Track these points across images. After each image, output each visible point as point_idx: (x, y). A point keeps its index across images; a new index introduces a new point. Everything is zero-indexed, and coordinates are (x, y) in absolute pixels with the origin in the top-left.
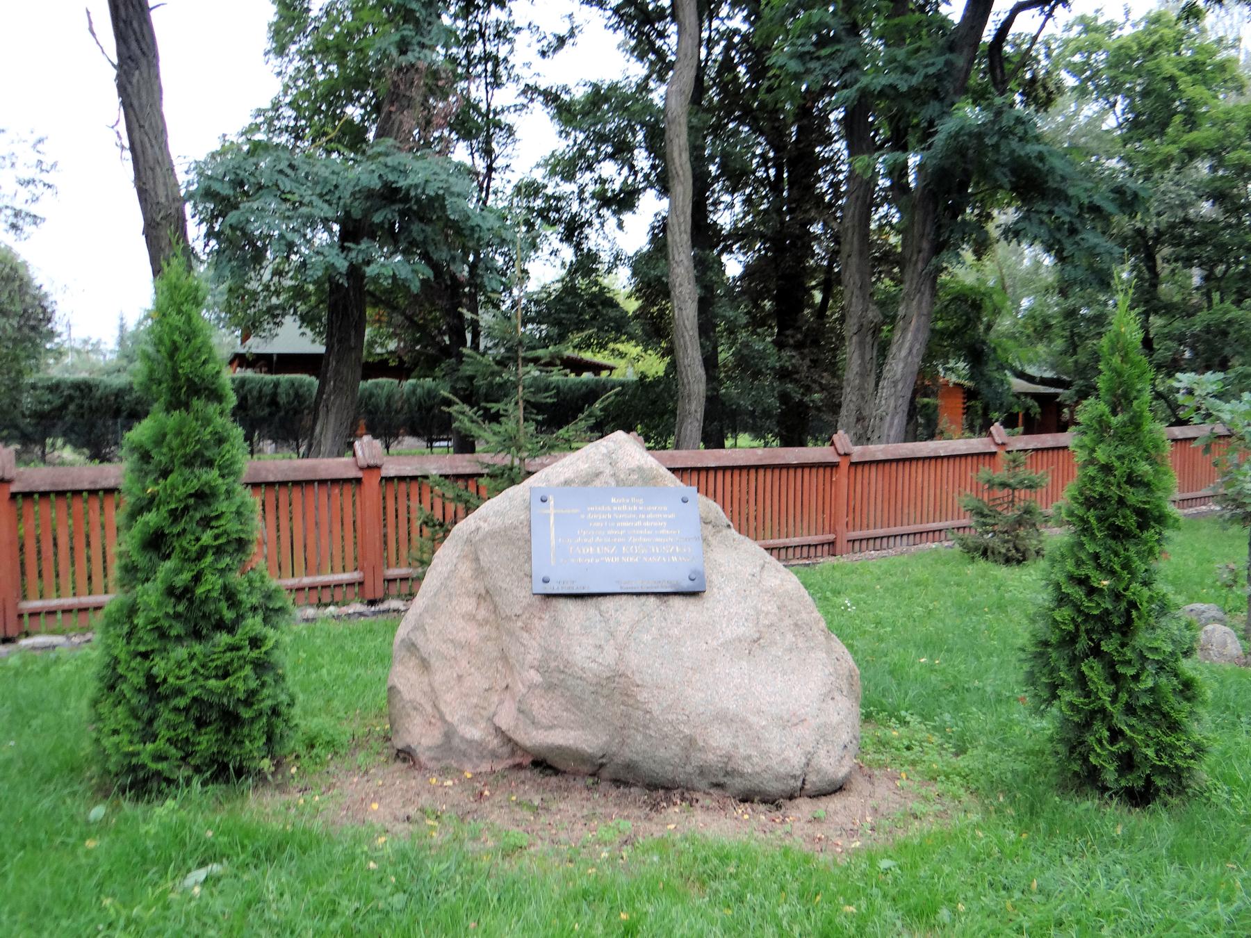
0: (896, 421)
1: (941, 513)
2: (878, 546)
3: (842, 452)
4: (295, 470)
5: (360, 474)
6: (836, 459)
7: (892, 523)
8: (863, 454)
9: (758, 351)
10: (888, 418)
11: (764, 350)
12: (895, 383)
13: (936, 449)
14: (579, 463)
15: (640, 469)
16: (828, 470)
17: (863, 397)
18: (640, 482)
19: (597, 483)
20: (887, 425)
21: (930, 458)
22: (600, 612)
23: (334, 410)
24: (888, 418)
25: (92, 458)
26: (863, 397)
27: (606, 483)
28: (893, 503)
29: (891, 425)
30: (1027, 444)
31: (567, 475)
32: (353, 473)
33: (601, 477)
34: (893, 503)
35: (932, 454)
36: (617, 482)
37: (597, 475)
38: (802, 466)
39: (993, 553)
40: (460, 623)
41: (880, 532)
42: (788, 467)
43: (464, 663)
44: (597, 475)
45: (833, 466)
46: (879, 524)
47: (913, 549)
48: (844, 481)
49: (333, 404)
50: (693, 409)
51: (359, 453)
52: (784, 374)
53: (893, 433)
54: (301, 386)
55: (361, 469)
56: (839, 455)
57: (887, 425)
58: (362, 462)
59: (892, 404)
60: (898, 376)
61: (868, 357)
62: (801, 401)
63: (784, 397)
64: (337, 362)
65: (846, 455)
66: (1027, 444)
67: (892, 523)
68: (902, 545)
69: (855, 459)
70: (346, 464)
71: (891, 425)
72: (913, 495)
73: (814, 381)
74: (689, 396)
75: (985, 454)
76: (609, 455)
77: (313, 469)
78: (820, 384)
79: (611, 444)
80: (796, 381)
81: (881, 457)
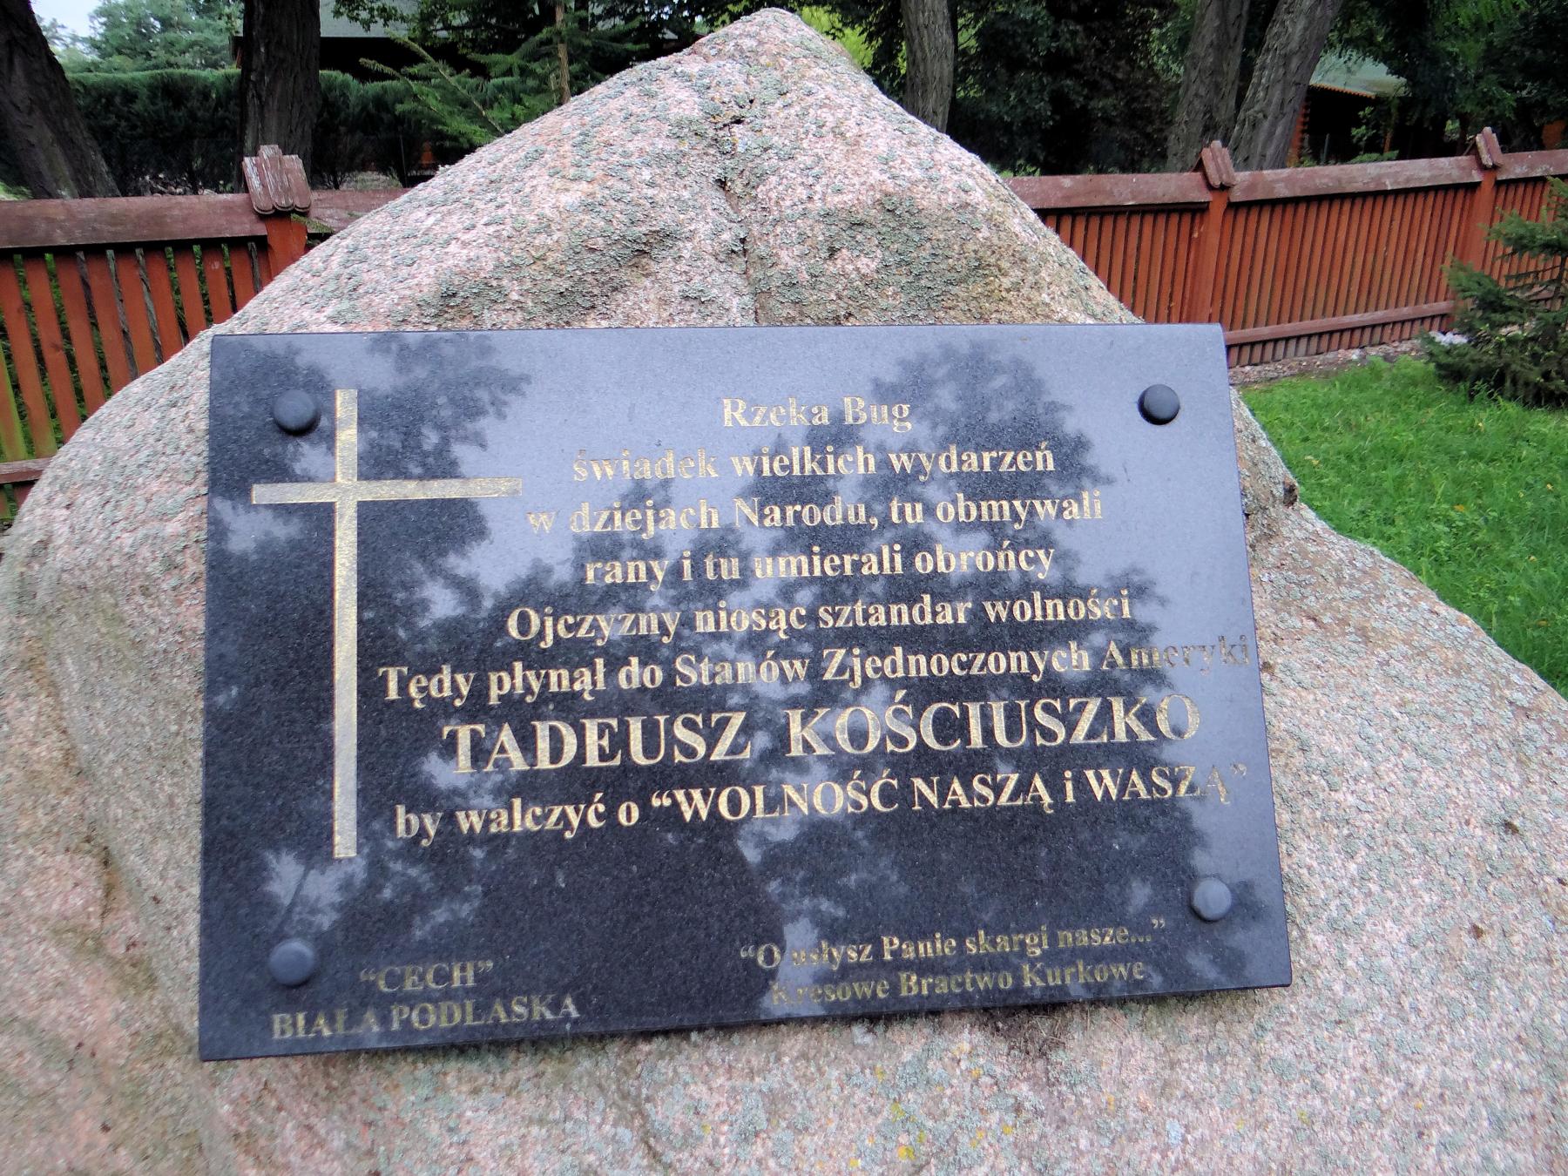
0: (1279, 130)
1: (1368, 296)
2: (1256, 358)
3: (1216, 183)
4: (115, 219)
5: (261, 230)
6: (1203, 196)
7: (1285, 316)
8: (1252, 187)
9: (1024, 21)
10: (1266, 124)
11: (1034, 21)
12: (1287, 58)
13: (1379, 178)
14: (538, 177)
15: (897, 214)
16: (1187, 219)
17: (1217, 86)
18: (890, 298)
19: (642, 300)
20: (1262, 136)
21: (1364, 195)
22: (648, 1140)
23: (274, 104)
24: (1266, 124)
25: (36, 196)
26: (1217, 86)
27: (696, 300)
28: (1291, 278)
29: (1271, 134)
30: (1532, 167)
31: (457, 256)
32: (246, 227)
33: (663, 267)
34: (1291, 278)
35: (1372, 187)
36: (760, 293)
37: (642, 250)
38: (1142, 210)
39: (1514, 382)
40: (54, 961)
41: (1265, 331)
42: (1116, 211)
43: (85, 1124)
44: (642, 250)
45: (1196, 210)
46: (1263, 318)
47: (1319, 360)
48: (1213, 239)
49: (271, 92)
50: (930, 107)
51: (254, 182)
52: (1058, 63)
53: (1270, 152)
54: (331, 88)
55: (263, 217)
56: (1210, 187)
57: (1262, 136)
58: (263, 203)
59: (1276, 96)
60: (1294, 45)
61: (1232, 15)
62: (1084, 107)
63: (1059, 101)
64: (267, 8)
65: (1224, 188)
66: (1532, 167)
67: (1285, 316)
68: (1297, 358)
69: (1237, 196)
70: (229, 209)
71: (1271, 134)
72: (1327, 263)
73: (1103, 75)
74: (924, 84)
75: (1456, 187)
76: (720, 126)
77: (156, 218)
78: (1113, 79)
79: (732, 71)
80: (1077, 75)
81: (1282, 192)
